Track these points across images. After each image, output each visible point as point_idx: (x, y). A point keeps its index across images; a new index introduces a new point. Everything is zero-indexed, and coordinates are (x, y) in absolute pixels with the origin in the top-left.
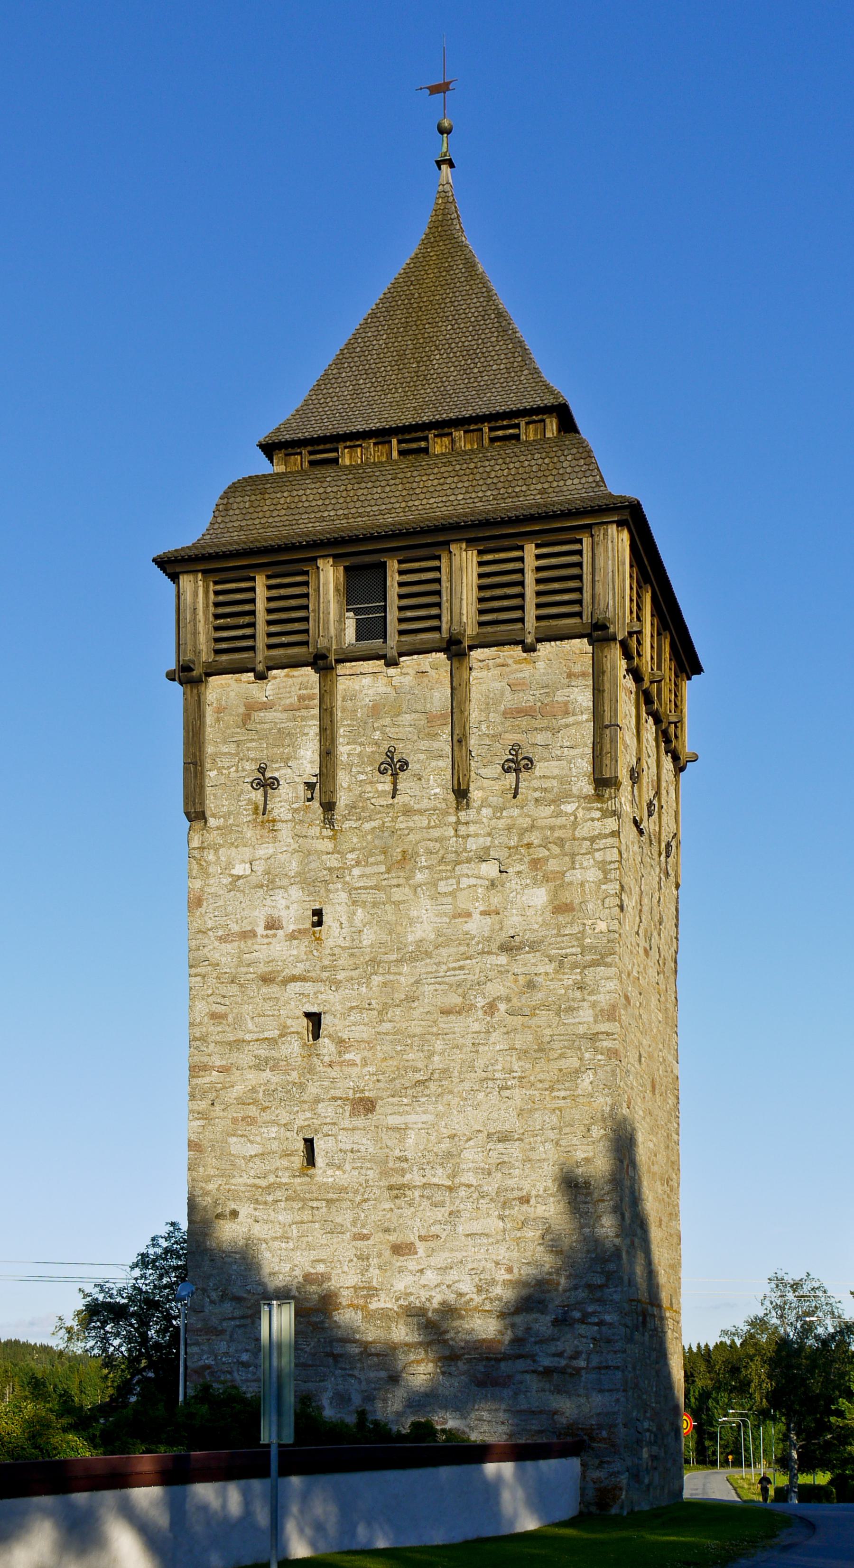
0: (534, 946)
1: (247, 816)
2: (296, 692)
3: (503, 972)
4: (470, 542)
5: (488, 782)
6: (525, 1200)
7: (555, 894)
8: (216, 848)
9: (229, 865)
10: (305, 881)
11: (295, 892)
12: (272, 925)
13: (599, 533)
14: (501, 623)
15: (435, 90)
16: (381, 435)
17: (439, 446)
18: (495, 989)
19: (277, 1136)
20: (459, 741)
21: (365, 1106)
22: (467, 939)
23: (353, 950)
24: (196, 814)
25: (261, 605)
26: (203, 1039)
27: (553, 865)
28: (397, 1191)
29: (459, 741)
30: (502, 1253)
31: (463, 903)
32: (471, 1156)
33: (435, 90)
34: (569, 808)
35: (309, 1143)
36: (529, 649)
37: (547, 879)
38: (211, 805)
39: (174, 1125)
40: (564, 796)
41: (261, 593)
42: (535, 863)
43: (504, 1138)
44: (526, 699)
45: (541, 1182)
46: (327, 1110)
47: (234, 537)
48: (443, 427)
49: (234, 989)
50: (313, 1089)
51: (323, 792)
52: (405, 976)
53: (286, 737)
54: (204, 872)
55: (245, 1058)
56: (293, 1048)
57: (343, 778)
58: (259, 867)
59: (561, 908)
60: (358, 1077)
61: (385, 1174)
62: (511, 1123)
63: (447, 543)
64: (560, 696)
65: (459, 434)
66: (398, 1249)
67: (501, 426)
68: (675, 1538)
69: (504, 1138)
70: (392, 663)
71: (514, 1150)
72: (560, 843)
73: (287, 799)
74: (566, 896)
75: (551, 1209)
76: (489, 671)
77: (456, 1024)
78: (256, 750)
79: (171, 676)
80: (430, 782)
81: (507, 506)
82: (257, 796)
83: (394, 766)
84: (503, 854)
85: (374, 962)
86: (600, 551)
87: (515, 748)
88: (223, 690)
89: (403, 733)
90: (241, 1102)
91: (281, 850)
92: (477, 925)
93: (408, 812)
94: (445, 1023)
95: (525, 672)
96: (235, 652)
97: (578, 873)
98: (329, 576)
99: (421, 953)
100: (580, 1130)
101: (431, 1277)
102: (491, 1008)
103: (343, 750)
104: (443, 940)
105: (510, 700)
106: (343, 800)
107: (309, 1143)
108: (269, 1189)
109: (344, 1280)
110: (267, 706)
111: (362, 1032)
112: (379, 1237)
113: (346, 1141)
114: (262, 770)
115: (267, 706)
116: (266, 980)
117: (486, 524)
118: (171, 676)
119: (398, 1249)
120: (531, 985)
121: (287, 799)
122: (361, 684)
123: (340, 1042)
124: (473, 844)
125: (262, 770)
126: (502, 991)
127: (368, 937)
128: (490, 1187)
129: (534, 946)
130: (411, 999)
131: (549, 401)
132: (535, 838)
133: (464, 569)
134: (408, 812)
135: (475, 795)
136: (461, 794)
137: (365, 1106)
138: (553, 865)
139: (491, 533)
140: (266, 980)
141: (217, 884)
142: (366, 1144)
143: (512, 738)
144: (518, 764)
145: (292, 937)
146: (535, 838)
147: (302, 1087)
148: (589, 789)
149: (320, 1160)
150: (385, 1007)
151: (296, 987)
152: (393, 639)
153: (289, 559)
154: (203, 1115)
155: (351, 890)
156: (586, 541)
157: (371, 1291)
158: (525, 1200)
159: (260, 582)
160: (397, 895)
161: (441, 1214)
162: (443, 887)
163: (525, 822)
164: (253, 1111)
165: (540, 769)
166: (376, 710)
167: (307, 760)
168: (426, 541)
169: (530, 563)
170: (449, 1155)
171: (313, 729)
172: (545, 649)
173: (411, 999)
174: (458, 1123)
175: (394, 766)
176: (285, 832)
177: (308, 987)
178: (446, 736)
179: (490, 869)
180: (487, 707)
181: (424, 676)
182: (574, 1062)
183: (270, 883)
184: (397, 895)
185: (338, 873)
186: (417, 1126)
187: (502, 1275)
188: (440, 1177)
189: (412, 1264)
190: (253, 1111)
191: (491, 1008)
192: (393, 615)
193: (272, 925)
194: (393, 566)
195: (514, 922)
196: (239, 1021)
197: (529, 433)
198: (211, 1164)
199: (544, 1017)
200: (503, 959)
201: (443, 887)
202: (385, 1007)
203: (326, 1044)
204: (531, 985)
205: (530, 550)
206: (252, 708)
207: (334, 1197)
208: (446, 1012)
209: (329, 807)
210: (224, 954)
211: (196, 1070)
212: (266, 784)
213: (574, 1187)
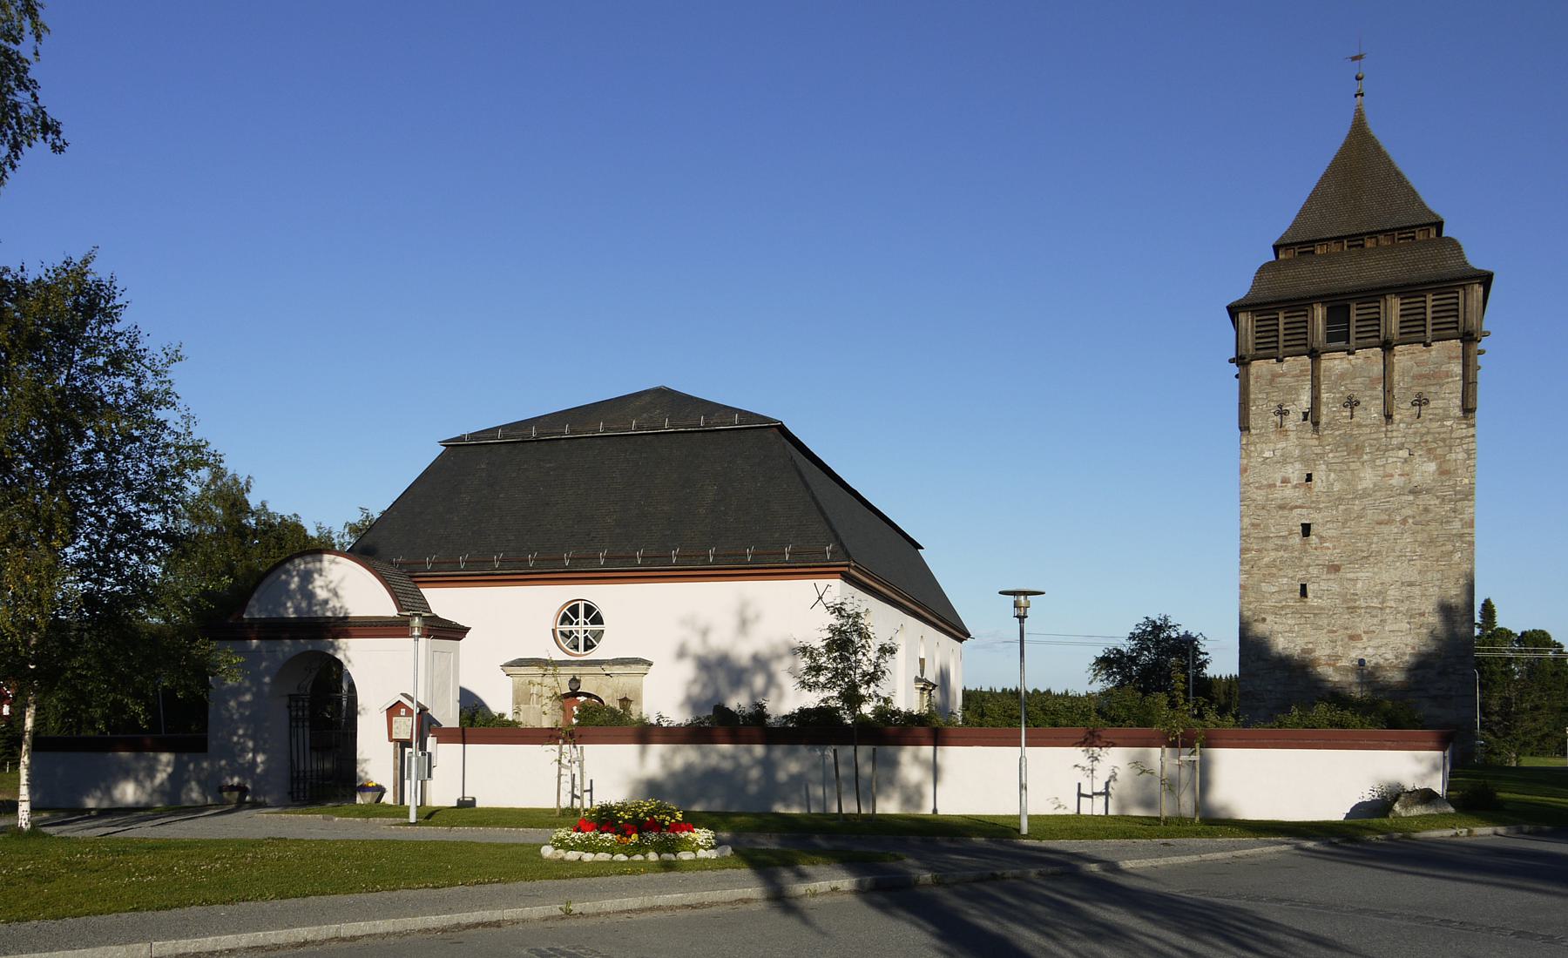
0: (1428, 491)
1: (1271, 428)
2: (1298, 368)
3: (1411, 504)
4: (1397, 294)
5: (1402, 411)
6: (1423, 614)
7: (1440, 466)
8: (1255, 444)
9: (1262, 452)
10: (1303, 459)
11: (1298, 465)
12: (1285, 481)
13: (1469, 289)
14: (1413, 332)
15: (1354, 58)
16: (1339, 239)
17: (1369, 244)
18: (1408, 512)
19: (1287, 581)
20: (1388, 391)
21: (1335, 568)
22: (1391, 487)
23: (1328, 493)
24: (1244, 427)
25: (1281, 327)
26: (1248, 536)
27: (1439, 451)
28: (1352, 610)
29: (1388, 391)
30: (1409, 640)
31: (1389, 470)
32: (1393, 593)
33: (1354, 58)
34: (1448, 423)
35: (1304, 587)
36: (1427, 345)
37: (1436, 458)
38: (1252, 423)
39: (1230, 576)
40: (1447, 417)
41: (1282, 321)
42: (1429, 451)
43: (1411, 584)
44: (1424, 370)
45: (1429, 606)
46: (1314, 571)
47: (1266, 295)
48: (1372, 234)
49: (1264, 512)
50: (1306, 560)
51: (1312, 417)
52: (1357, 506)
53: (1294, 391)
54: (1249, 456)
55: (1270, 545)
56: (1297, 540)
57: (1324, 410)
58: (1278, 453)
59: (1443, 472)
60: (1332, 554)
61: (1345, 601)
62: (1415, 577)
63: (1384, 296)
64: (1444, 368)
65: (1381, 237)
66: (1352, 638)
67: (1407, 231)
68: (609, 904)
69: (1411, 584)
70: (1351, 353)
71: (1417, 590)
72: (1444, 440)
73: (1293, 420)
74: (1446, 467)
75: (1434, 620)
76: (1404, 357)
77: (1385, 529)
78: (1277, 397)
79: (1231, 361)
80: (1375, 411)
81: (1416, 276)
82: (1277, 419)
83: (1352, 403)
84: (1411, 446)
85: (1340, 498)
86: (1469, 297)
87: (1419, 395)
88: (1257, 367)
89: (1356, 386)
90: (1267, 566)
91: (1291, 444)
92: (1396, 481)
93: (1359, 426)
94: (1378, 528)
95: (1426, 356)
96: (1269, 348)
97: (1453, 456)
98: (1319, 312)
99: (1366, 494)
100: (1453, 581)
101: (1370, 651)
102: (1404, 521)
103: (1324, 396)
104: (1377, 488)
105: (1416, 370)
106: (1323, 420)
107: (1304, 587)
108: (1283, 608)
109: (1322, 652)
110: (1283, 375)
111: (1332, 533)
112: (1341, 632)
113: (1324, 586)
114: (1280, 406)
115: (1283, 375)
116: (1282, 507)
117: (1408, 285)
118: (1231, 361)
119: (1352, 638)
120: (1426, 510)
121: (1293, 420)
122: (1335, 363)
123: (1321, 538)
124: (1394, 442)
125: (1280, 406)
126: (1410, 512)
127: (1337, 487)
128: (1403, 608)
129: (1428, 491)
130: (1360, 517)
131: (1433, 220)
132: (1429, 438)
133: (1394, 306)
134: (1359, 426)
135: (1397, 417)
136: (1389, 417)
137: (1335, 568)
138: (1439, 451)
139: (1406, 290)
140: (1282, 507)
141: (1255, 461)
142: (1335, 587)
143: (1419, 389)
144: (1420, 402)
145: (1295, 487)
146: (1429, 438)
147: (1300, 559)
148: (1460, 414)
149: (1310, 595)
150: (1346, 521)
151: (1298, 511)
152: (1353, 342)
153: (1298, 305)
154: (1246, 572)
155: (1328, 464)
156: (1461, 293)
157: (1338, 658)
158: (1423, 614)
159: (1281, 316)
160: (1353, 466)
161: (1375, 621)
162: (1378, 462)
163: (1424, 430)
164: (1274, 571)
165: (1432, 404)
166: (1342, 376)
167: (1305, 401)
168: (1374, 294)
169: (1429, 304)
170: (1380, 592)
171: (1308, 386)
172: (1436, 345)
173: (1360, 517)
174: (1385, 577)
175: (1352, 403)
176: (1292, 436)
177: (1304, 511)
178: (1380, 388)
179: (1404, 454)
180: (1403, 375)
181: (1369, 360)
182: (1450, 548)
183: (1285, 460)
184: (1353, 466)
185: (1321, 456)
186: (1363, 579)
187: (1409, 650)
188: (1375, 603)
189: (1360, 645)
190: (1274, 571)
191: (1404, 521)
192: (1353, 330)
193: (1285, 481)
194: (1353, 306)
195: (1417, 479)
196: (1267, 527)
197: (1420, 236)
198: (1252, 596)
199: (1433, 525)
200: (1411, 498)
201: (1378, 462)
202: (1346, 521)
203: (1313, 538)
204: (1426, 510)
205: (1430, 297)
206: (1274, 376)
207: (1318, 612)
208: (1380, 523)
209: (1316, 424)
210: (1260, 496)
211: (1243, 551)
212: (1282, 413)
213: (1446, 610)
